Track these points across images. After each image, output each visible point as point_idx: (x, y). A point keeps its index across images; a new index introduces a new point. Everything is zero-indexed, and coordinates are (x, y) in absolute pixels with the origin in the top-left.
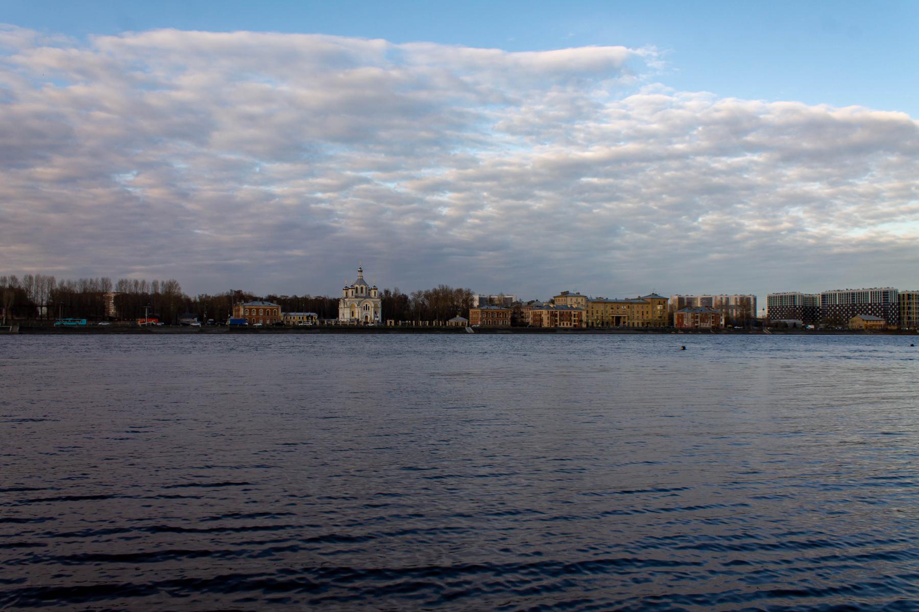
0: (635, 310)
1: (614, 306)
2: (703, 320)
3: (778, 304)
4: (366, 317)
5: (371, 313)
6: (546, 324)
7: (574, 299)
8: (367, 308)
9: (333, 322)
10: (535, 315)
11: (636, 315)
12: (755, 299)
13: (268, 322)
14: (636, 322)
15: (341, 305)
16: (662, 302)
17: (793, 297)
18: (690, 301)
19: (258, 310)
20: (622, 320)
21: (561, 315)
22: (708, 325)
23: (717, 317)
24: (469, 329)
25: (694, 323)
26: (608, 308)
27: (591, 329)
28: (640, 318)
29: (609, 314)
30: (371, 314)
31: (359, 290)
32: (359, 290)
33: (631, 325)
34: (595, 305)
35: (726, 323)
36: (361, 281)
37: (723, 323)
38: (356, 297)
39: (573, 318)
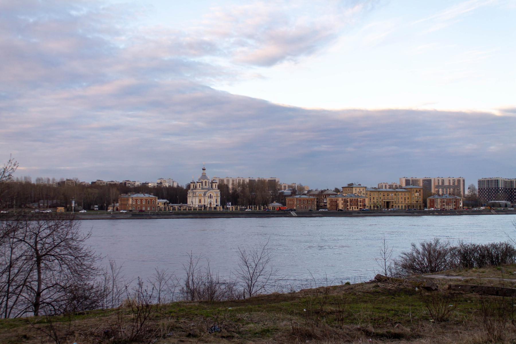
0: (400, 197)
1: (386, 194)
2: (448, 204)
3: (486, 186)
4: (210, 203)
5: (213, 199)
6: (341, 207)
7: (358, 190)
8: (211, 197)
9: (184, 206)
10: (332, 201)
11: (400, 200)
12: (464, 181)
13: (149, 209)
14: (400, 205)
15: (190, 194)
16: (418, 191)
17: (497, 181)
18: (415, 182)
19: (141, 200)
20: (391, 204)
21: (351, 201)
22: (451, 207)
23: (457, 202)
24: (293, 213)
25: (442, 206)
26: (381, 196)
27: (365, 212)
28: (403, 202)
29: (377, 199)
30: (213, 200)
31: (204, 184)
32: (204, 184)
33: (400, 208)
34: (372, 193)
35: (463, 206)
36: (204, 176)
37: (461, 205)
38: (202, 189)
39: (359, 204)
